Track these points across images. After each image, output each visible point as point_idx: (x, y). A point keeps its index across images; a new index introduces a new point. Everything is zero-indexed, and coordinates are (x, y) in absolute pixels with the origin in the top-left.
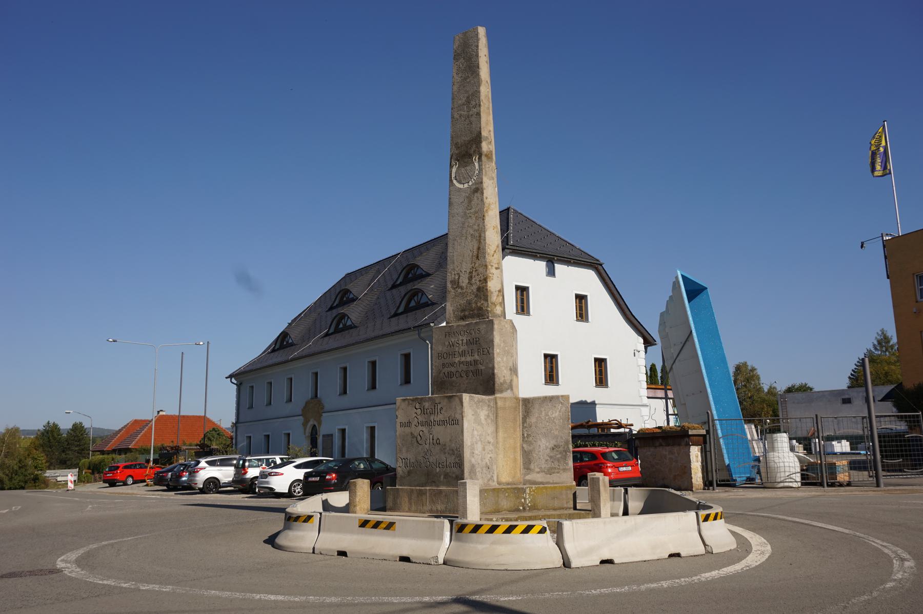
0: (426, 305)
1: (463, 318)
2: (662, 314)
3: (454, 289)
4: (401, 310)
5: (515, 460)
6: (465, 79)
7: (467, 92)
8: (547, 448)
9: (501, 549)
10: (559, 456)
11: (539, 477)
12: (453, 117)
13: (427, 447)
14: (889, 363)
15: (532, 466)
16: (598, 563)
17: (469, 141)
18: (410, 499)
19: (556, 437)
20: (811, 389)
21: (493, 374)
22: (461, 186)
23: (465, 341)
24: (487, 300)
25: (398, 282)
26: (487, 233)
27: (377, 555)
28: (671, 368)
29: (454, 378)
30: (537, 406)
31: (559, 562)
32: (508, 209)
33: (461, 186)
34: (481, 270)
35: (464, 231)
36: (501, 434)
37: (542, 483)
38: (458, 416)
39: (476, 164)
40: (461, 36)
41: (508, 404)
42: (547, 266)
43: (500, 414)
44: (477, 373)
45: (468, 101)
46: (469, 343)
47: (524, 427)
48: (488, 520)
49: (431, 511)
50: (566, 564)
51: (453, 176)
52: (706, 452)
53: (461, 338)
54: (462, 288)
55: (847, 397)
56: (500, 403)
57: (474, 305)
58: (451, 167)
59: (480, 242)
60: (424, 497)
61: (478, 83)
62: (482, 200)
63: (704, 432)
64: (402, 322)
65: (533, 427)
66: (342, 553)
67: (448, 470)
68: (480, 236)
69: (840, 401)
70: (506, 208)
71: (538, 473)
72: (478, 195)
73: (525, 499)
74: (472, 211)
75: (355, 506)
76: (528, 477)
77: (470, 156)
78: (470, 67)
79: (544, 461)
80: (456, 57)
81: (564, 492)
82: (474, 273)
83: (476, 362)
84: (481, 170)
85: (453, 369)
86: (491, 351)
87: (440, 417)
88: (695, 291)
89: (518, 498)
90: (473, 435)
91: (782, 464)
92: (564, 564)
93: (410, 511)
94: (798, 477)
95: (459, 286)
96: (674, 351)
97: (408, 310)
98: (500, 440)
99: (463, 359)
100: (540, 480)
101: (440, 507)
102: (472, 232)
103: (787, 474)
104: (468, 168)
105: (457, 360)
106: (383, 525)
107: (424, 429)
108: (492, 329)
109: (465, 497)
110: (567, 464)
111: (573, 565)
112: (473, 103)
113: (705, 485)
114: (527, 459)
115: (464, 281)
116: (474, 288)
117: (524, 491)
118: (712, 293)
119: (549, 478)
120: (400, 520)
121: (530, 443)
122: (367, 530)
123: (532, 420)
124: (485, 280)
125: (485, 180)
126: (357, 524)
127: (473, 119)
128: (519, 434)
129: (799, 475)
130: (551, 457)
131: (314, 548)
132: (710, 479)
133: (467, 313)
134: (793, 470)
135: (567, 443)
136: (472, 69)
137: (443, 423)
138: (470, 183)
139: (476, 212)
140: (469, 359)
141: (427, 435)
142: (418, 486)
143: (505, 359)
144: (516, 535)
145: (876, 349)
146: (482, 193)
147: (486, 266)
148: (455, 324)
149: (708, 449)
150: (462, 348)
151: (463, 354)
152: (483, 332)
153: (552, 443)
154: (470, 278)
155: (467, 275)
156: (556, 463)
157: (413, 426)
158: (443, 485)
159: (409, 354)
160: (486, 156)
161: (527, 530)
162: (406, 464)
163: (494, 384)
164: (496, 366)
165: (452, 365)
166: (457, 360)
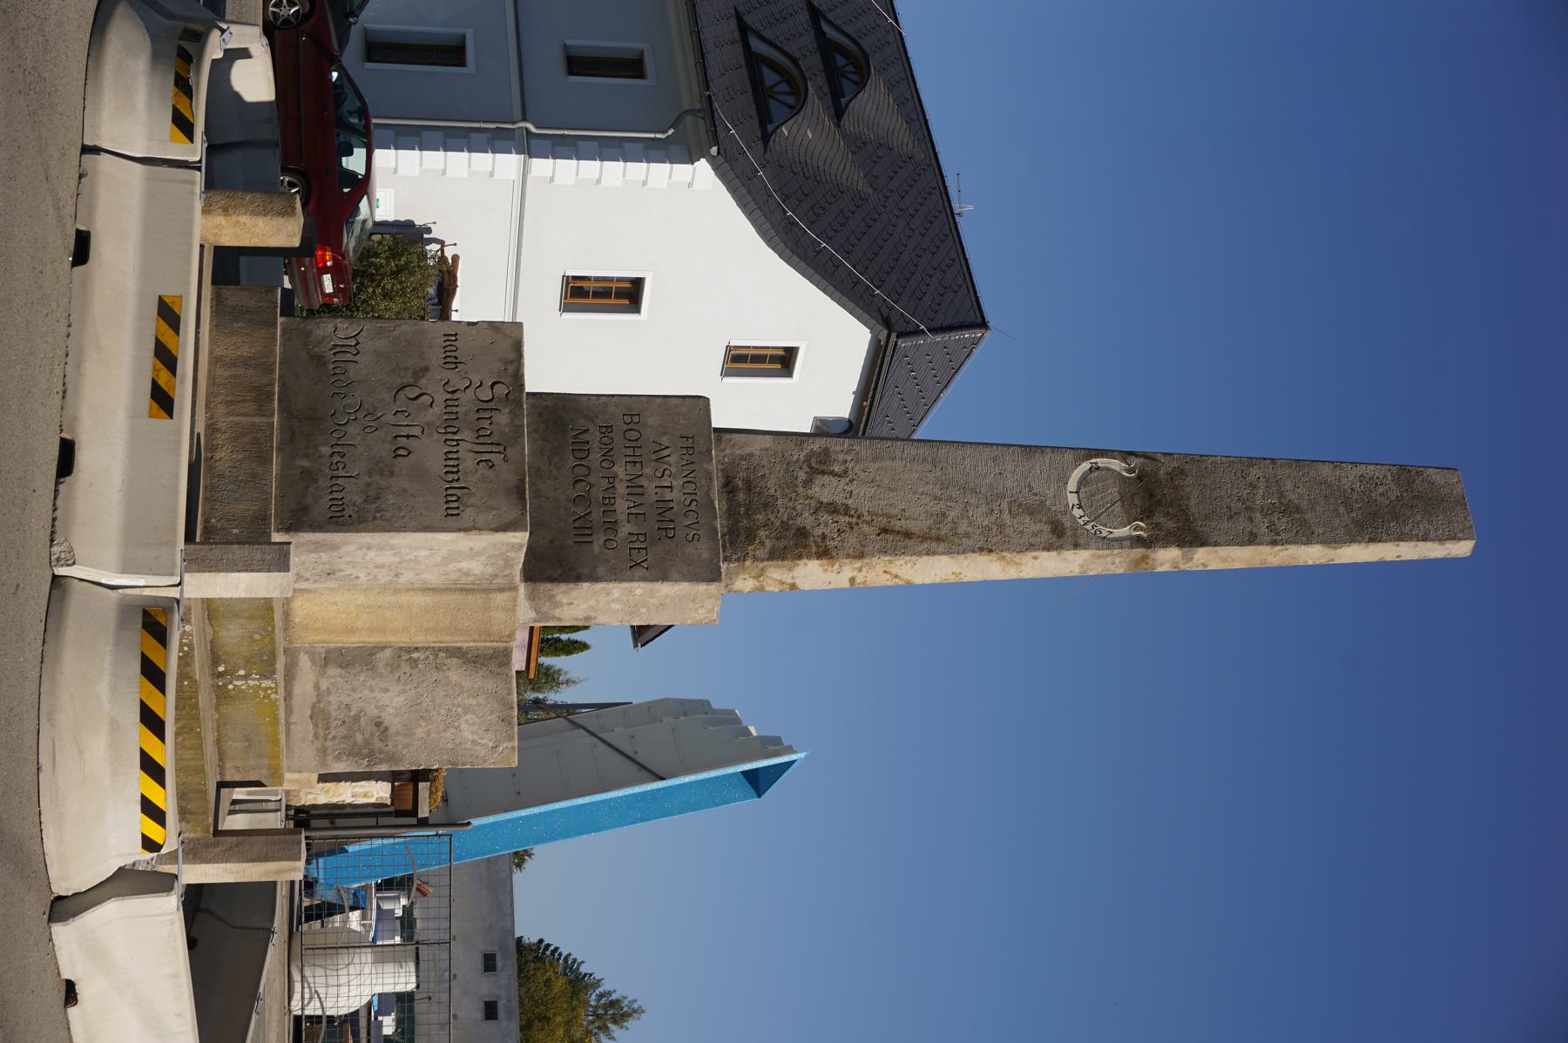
0: (765, 118)
1: (729, 486)
2: (703, 706)
3: (807, 461)
4: (756, 44)
5: (351, 630)
6: (1346, 502)
7: (1313, 505)
8: (381, 708)
9: (98, 749)
10: (359, 738)
11: (304, 687)
12: (1252, 462)
13: (389, 418)
14: (568, 1023)
15: (333, 671)
16: (66, 975)
17: (1184, 511)
18: (246, 362)
19: (409, 733)
20: (519, 866)
21: (578, 579)
22: (1072, 485)
23: (668, 496)
24: (773, 556)
25: (826, 28)
26: (945, 558)
27: (78, 366)
28: (578, 726)
29: (572, 462)
30: (490, 685)
31: (64, 885)
32: (983, 325)
33: (1072, 485)
34: (852, 540)
35: (955, 493)
36: (420, 599)
37: (288, 697)
38: (468, 515)
39: (1124, 531)
40: (1458, 489)
41: (499, 616)
42: (839, 421)
43: (478, 599)
44: (584, 530)
45: (1288, 509)
46: (664, 507)
47: (436, 651)
48: (185, 660)
49: (211, 428)
50: (63, 908)
51: (1102, 462)
52: (376, 815)
53: (678, 483)
54: (808, 483)
55: (499, 963)
56: (500, 598)
57: (760, 517)
58: (1125, 455)
59: (924, 538)
60: (250, 407)
61: (1330, 541)
62: (1031, 547)
63: (424, 812)
64: (725, 56)
65: (436, 675)
66: (82, 249)
67: (324, 483)
68: (938, 539)
69: (490, 950)
70: (988, 317)
71: (317, 686)
72: (1046, 535)
73: (246, 677)
74: (1006, 516)
75: (226, 211)
76: (304, 660)
77: (1146, 514)
78: (1375, 515)
79: (347, 700)
80: (1405, 473)
81: (265, 762)
82: (844, 520)
83: (612, 527)
84: (1109, 543)
85: (595, 457)
86: (639, 572)
87: (469, 462)
88: (758, 782)
89: (248, 662)
90: (418, 548)
91: (343, 980)
92: (60, 898)
93: (215, 360)
94: (313, 1009)
95: (814, 472)
96: (618, 736)
97: (754, 62)
98: (405, 599)
99: (621, 489)
100: (297, 691)
101: (224, 457)
102: (952, 515)
103: (322, 991)
104: (1117, 508)
105: (619, 470)
106: (164, 378)
107: (438, 409)
108: (695, 578)
109: (248, 568)
110: (338, 758)
111: (58, 930)
112: (1282, 524)
113: (300, 810)
114: (353, 659)
115: (826, 490)
116: (806, 520)
117: (268, 673)
118: (753, 804)
119: (301, 713)
120: (179, 431)
121: (393, 666)
122: (152, 324)
123: (456, 673)
124: (824, 554)
125: (1083, 555)
126: (168, 291)
127: (1242, 524)
128: (419, 639)
129: (319, 1012)
130: (356, 718)
131: (96, 150)
132: (314, 823)
133: (741, 496)
134: (329, 1003)
135: (392, 758)
136: (1371, 522)
137: (453, 469)
138: (1077, 512)
139: (1001, 527)
140: (622, 506)
141: (421, 420)
142: (283, 386)
143: (616, 606)
144: (137, 736)
145: (601, 996)
146: (1048, 548)
147: (861, 556)
148: (714, 466)
149: (383, 821)
150: (650, 486)
151: (636, 489)
152: (690, 550)
153: (394, 724)
154: (832, 508)
155: (840, 499)
156: (343, 731)
157: (448, 374)
158: (285, 466)
159: (641, 76)
160: (1144, 558)
161: (151, 810)
162: (339, 349)
163: (551, 580)
164: (600, 586)
165: (608, 456)
166: (619, 470)
